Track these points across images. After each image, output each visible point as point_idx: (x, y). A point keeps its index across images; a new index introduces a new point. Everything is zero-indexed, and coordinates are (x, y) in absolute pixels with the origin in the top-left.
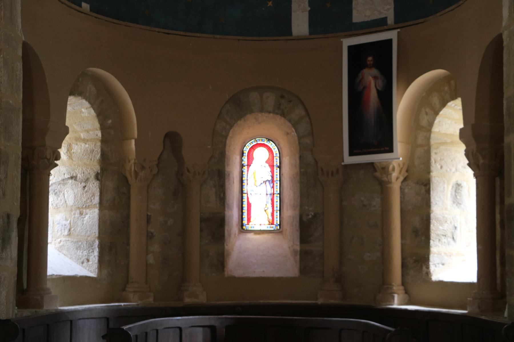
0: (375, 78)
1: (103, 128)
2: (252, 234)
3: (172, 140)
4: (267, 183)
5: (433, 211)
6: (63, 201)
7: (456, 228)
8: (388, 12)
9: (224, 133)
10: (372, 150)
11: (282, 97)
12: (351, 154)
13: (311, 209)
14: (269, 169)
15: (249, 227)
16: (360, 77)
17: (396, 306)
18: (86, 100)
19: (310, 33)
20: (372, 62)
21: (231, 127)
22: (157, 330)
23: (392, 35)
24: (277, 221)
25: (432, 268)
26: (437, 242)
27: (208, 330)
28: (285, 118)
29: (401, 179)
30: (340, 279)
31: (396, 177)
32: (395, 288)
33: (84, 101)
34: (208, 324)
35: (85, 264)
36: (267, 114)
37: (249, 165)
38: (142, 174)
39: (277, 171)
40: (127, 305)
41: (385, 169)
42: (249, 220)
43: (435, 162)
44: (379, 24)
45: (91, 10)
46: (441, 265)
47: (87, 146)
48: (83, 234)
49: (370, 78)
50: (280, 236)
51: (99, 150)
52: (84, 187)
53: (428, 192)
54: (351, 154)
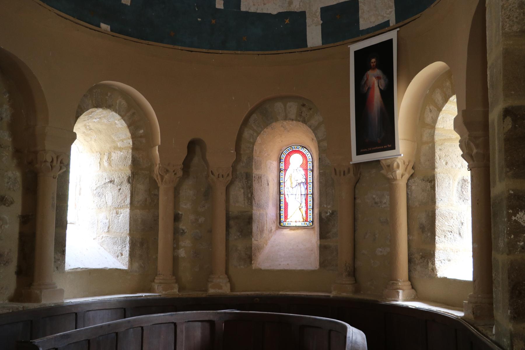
0: (378, 78)
1: (134, 137)
2: (288, 229)
3: (194, 146)
4: (302, 185)
5: (438, 207)
6: (105, 202)
7: (462, 224)
8: (389, 15)
9: (251, 140)
10: (376, 148)
11: (304, 105)
12: (358, 153)
13: (329, 207)
14: (303, 172)
15: (286, 224)
16: (365, 79)
17: (401, 302)
18: (116, 112)
19: (323, 44)
20: (375, 64)
21: (258, 134)
22: (142, 328)
23: (392, 35)
24: (310, 218)
25: (438, 264)
26: (442, 238)
27: (207, 325)
28: (306, 124)
29: (407, 176)
30: (353, 273)
31: (401, 174)
32: (400, 284)
33: (114, 113)
34: (207, 319)
35: (119, 257)
36: (291, 122)
37: (286, 170)
38: (166, 177)
39: (310, 174)
40: (148, 296)
41: (390, 167)
42: (286, 217)
43: (440, 159)
44: (384, 27)
45: (112, 30)
46: (446, 261)
47: (122, 153)
48: (118, 231)
49: (374, 79)
50: (312, 232)
51: (131, 157)
52: (120, 189)
53: (433, 188)
54: (358, 153)
